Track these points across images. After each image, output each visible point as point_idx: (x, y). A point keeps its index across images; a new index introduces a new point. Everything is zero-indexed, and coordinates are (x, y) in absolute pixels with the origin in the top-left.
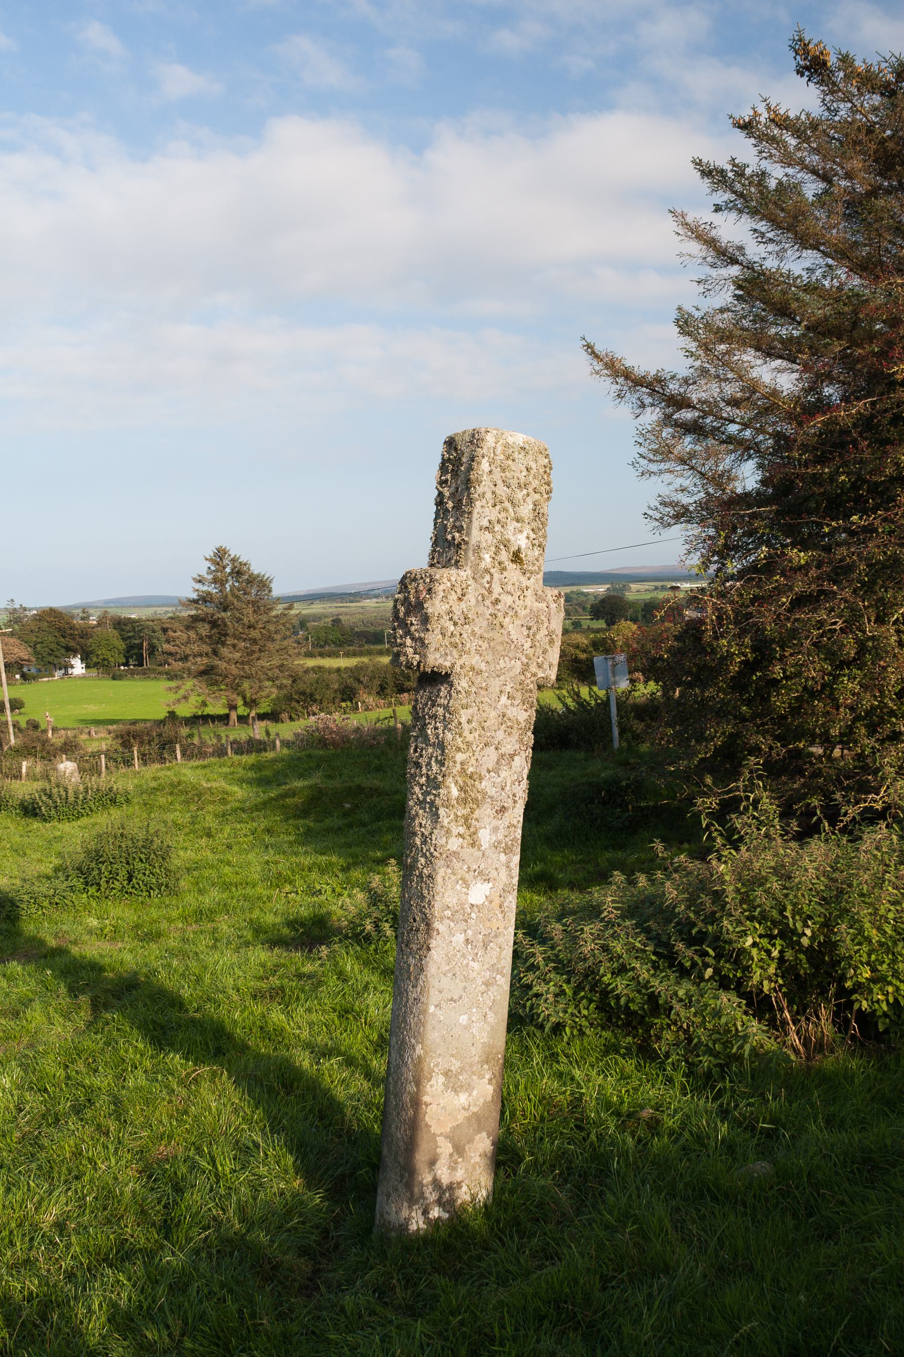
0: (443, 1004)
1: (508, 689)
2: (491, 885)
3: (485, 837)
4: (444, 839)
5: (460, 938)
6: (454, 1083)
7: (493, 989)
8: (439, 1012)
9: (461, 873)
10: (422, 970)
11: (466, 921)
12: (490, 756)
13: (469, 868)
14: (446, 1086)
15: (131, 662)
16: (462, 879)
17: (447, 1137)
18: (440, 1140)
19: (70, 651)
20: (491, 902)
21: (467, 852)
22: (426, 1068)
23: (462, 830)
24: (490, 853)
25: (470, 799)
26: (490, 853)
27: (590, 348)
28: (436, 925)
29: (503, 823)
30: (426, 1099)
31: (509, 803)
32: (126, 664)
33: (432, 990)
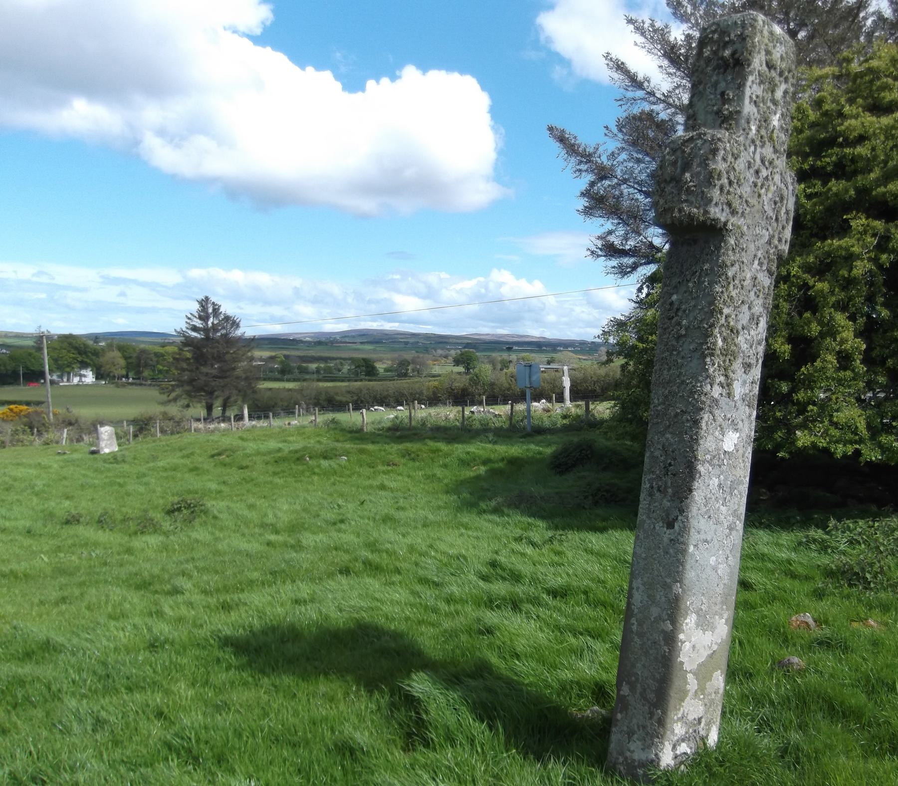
0: (700, 545)
1: (759, 255)
2: (738, 435)
3: (738, 389)
4: (709, 387)
5: (716, 481)
6: (705, 624)
7: (734, 533)
8: (696, 553)
9: (720, 420)
10: (682, 511)
11: (720, 467)
12: (744, 319)
13: (725, 416)
14: (697, 625)
15: (131, 374)
16: (720, 426)
17: (694, 674)
18: (690, 676)
19: (84, 365)
20: (737, 451)
21: (723, 401)
22: (683, 606)
23: (722, 379)
24: (739, 403)
25: (730, 353)
26: (739, 403)
27: (562, 139)
28: (700, 468)
29: (749, 378)
30: (682, 636)
31: (753, 361)
32: (127, 377)
33: (692, 530)
